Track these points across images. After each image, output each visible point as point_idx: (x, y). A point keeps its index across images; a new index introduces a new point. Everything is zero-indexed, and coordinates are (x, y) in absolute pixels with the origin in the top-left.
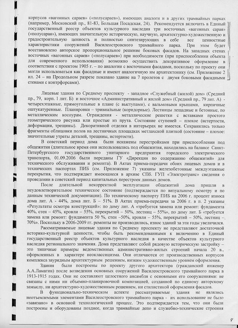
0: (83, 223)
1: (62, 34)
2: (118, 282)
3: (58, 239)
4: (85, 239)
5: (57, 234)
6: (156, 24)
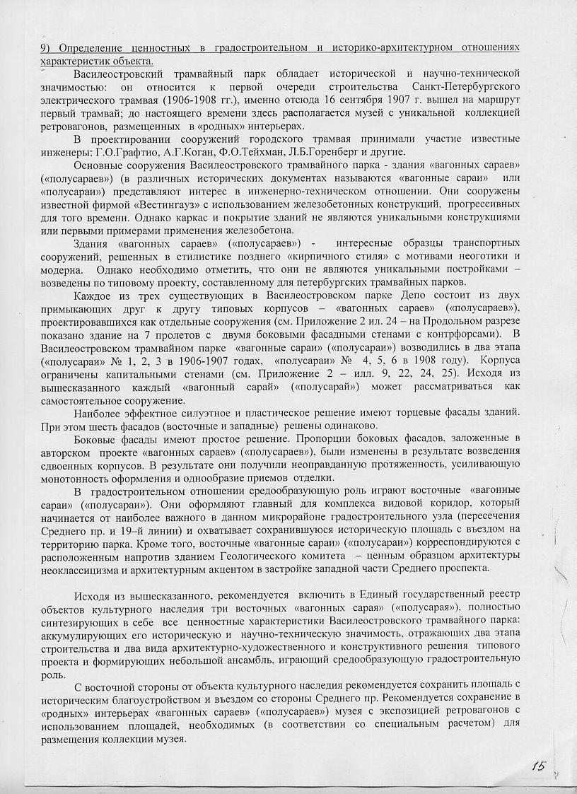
1: (173, 439)
3: (392, 594)
4: (49, 611)
5: (263, 686)
6: (387, 699)
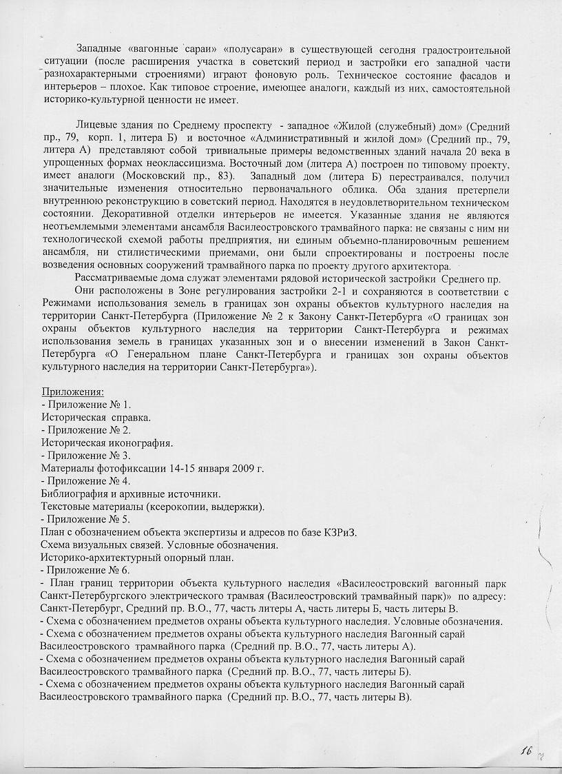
0: (246, 470)
2: (159, 240)
3: (155, 558)
6: (47, 304)
